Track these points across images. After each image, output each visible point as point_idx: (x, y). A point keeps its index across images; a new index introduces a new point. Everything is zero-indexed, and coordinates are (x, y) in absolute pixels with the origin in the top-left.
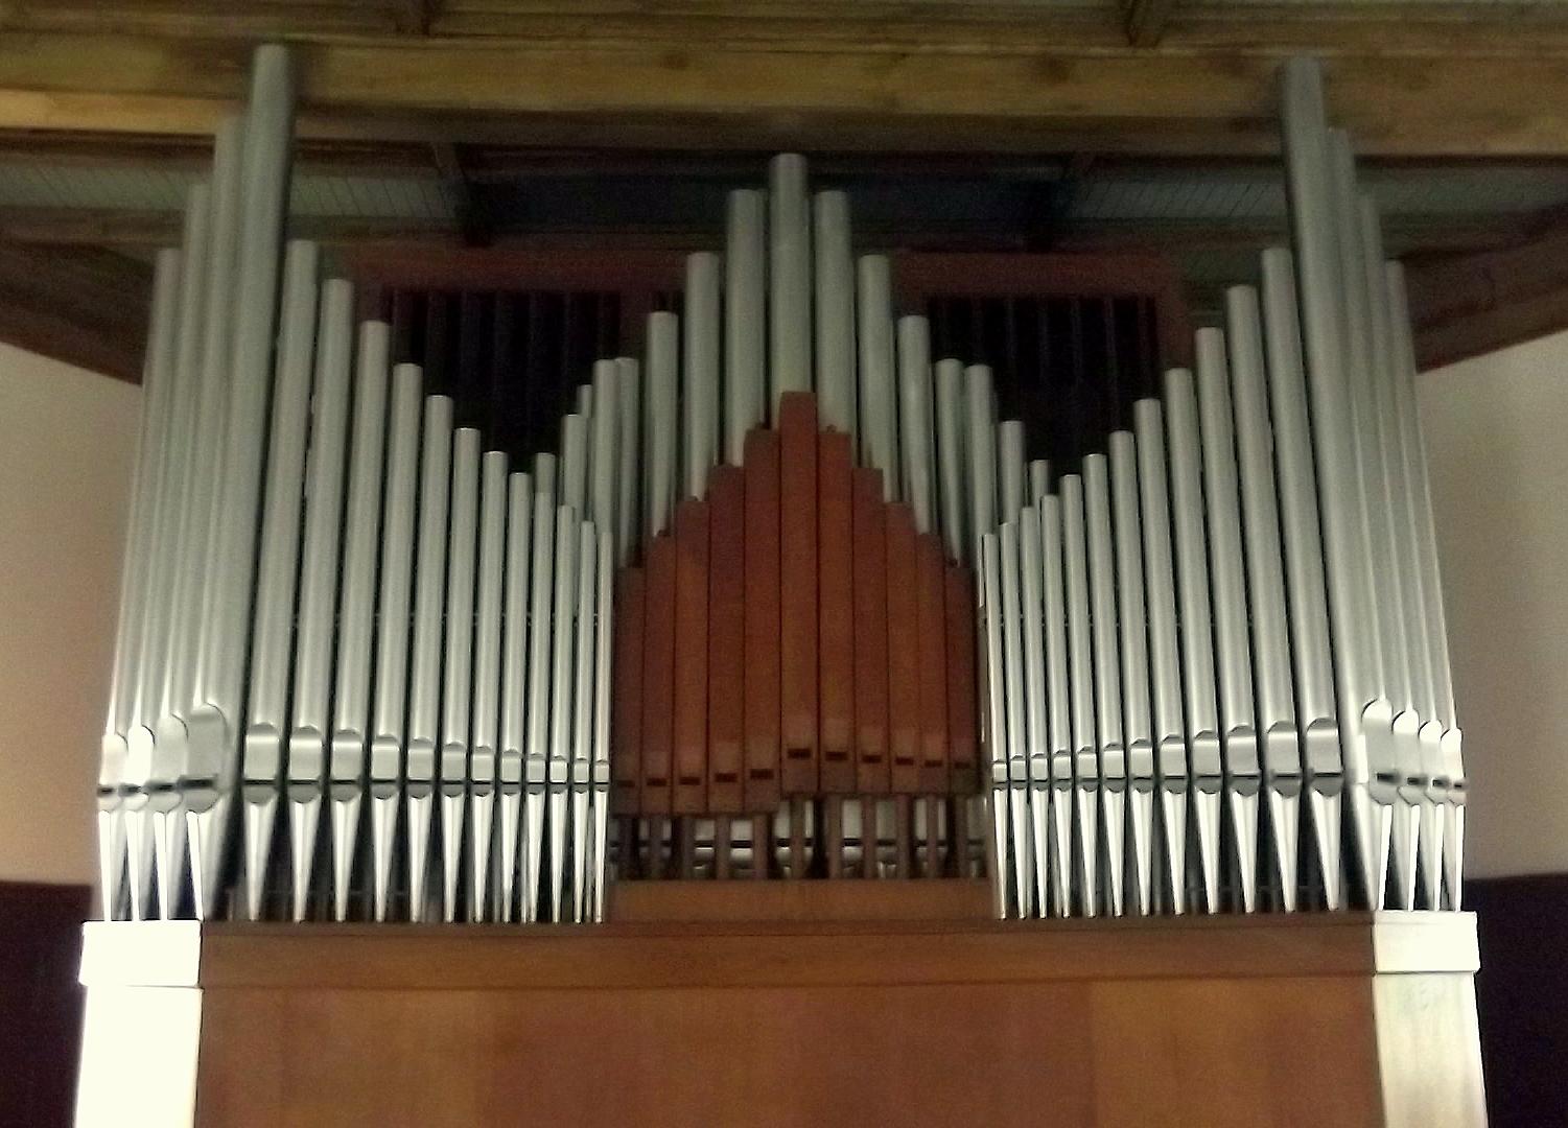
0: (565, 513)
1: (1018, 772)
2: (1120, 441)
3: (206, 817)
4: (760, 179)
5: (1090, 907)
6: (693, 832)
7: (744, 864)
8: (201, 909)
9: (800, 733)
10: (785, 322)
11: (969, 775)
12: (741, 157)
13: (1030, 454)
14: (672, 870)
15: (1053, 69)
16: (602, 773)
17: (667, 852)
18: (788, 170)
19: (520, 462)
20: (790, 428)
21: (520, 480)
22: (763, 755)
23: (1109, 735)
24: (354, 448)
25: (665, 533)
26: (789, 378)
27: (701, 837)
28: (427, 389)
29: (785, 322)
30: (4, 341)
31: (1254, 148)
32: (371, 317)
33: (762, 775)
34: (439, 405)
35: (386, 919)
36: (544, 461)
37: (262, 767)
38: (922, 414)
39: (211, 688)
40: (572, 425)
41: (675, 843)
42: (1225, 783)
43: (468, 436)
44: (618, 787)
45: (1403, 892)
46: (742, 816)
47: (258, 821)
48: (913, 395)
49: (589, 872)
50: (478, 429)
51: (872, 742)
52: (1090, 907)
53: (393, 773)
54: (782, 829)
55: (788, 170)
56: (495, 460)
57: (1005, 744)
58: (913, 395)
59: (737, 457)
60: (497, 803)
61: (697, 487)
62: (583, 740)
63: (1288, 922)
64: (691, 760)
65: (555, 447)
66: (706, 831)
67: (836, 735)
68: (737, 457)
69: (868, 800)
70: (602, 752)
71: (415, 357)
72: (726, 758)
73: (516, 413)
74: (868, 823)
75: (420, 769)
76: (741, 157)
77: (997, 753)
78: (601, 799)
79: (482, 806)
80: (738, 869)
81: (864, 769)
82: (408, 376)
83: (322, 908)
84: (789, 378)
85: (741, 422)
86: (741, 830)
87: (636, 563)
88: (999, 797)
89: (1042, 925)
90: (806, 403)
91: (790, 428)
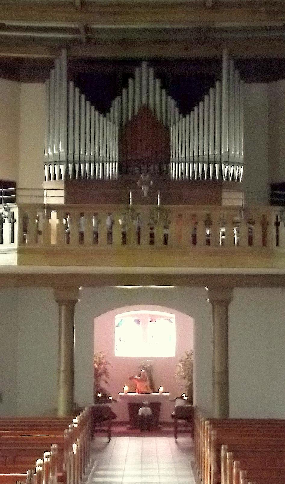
2: (191, 113)
9: (145, 154)
10: (146, 91)
12: (136, 62)
13: (180, 113)
15: (185, 49)
16: (117, 160)
18: (144, 65)
20: (145, 109)
21: (105, 119)
22: (139, 157)
23: (186, 154)
26: (144, 101)
28: (91, 105)
29: (146, 91)
30: (2, 77)
31: (218, 62)
37: (71, 159)
42: (74, 163)
48: (163, 102)
53: (78, 160)
55: (144, 65)
58: (163, 102)
62: (113, 152)
65: (109, 112)
71: (243, 469)
73: (103, 108)
76: (136, 62)
85: (136, 109)
87: (122, 129)
91: (145, 109)
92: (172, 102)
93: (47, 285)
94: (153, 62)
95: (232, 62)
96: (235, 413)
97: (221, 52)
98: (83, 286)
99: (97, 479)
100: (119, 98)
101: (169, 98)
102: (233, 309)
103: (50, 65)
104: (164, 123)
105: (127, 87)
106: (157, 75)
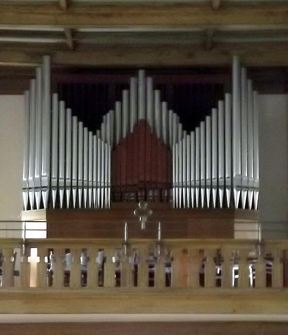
0: (102, 142)
1: (177, 185)
3: (45, 193)
4: (136, 75)
5: (102, 207)
6: (124, 195)
7: (132, 200)
8: (45, 207)
9: (142, 178)
11: (170, 186)
12: (132, 71)
14: (121, 200)
16: (109, 185)
17: (120, 198)
18: (141, 73)
19: (94, 133)
20: (142, 125)
23: (192, 178)
24: (53, 118)
25: (119, 144)
26: (141, 117)
27: (125, 196)
31: (227, 70)
32: (54, 92)
33: (135, 185)
34: (81, 124)
35: (55, 208)
36: (98, 132)
38: (165, 119)
39: (45, 172)
40: (103, 125)
41: (121, 197)
43: (86, 129)
44: (112, 188)
45: (243, 202)
46: (132, 192)
47: (54, 193)
49: (96, 202)
50: (71, 108)
51: (154, 179)
52: (102, 207)
54: (139, 194)
55: (141, 73)
56: (91, 133)
57: (175, 180)
59: (132, 131)
60: (97, 189)
61: (124, 136)
63: (221, 210)
64: (124, 183)
65: (100, 129)
66: (126, 195)
67: (148, 179)
68: (132, 131)
69: (154, 189)
70: (109, 181)
72: (130, 183)
73: (93, 124)
74: (153, 194)
75: (74, 183)
77: (174, 182)
78: (109, 189)
79: (90, 190)
80: (131, 201)
81: (152, 184)
82: (86, 129)
83: (50, 206)
84: (141, 117)
86: (132, 194)
87: (114, 149)
88: (174, 189)
89: (177, 210)
90: (145, 122)
91: (142, 125)
94: (150, 71)
101: (171, 112)
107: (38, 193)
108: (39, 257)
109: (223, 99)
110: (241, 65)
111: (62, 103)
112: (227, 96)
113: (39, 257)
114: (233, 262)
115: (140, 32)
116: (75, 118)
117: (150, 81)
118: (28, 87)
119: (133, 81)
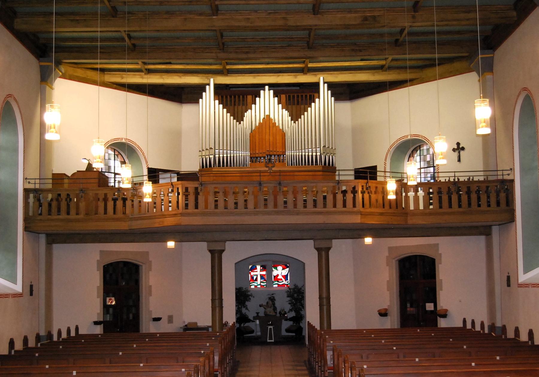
12: (262, 86)
18: (267, 88)
20: (267, 119)
26: (267, 113)
31: (316, 86)
36: (242, 122)
55: (267, 88)
59: (261, 121)
61: (257, 124)
65: (243, 121)
76: (262, 86)
91: (267, 119)
92: (286, 113)
93: (481, 234)
94: (272, 86)
95: (326, 85)
96: (483, 238)
97: (319, 79)
98: (374, 236)
99: (242, 374)
100: (249, 111)
101: (284, 110)
102: (332, 254)
103: (200, 89)
104: (281, 128)
105: (255, 104)
106: (275, 95)
107: (112, 184)
108: (440, 252)
109: (314, 102)
110: (324, 83)
111: (221, 106)
112: (317, 100)
113: (440, 252)
114: (372, 183)
115: (112, 242)
116: (229, 114)
117: (272, 92)
118: (198, 102)
119: (262, 92)
